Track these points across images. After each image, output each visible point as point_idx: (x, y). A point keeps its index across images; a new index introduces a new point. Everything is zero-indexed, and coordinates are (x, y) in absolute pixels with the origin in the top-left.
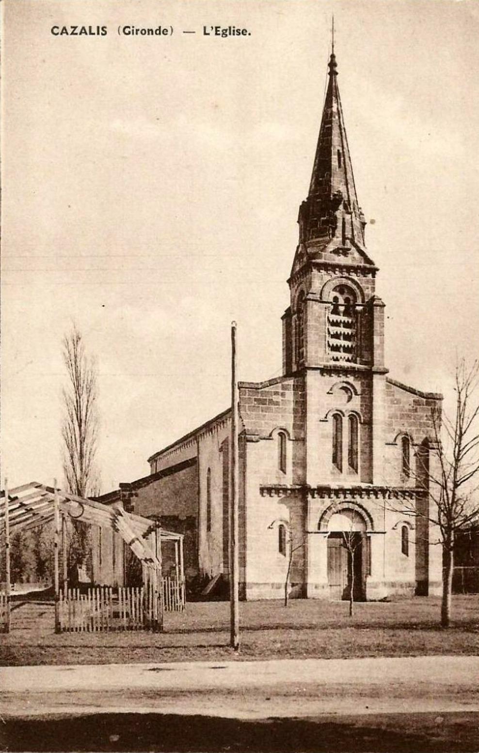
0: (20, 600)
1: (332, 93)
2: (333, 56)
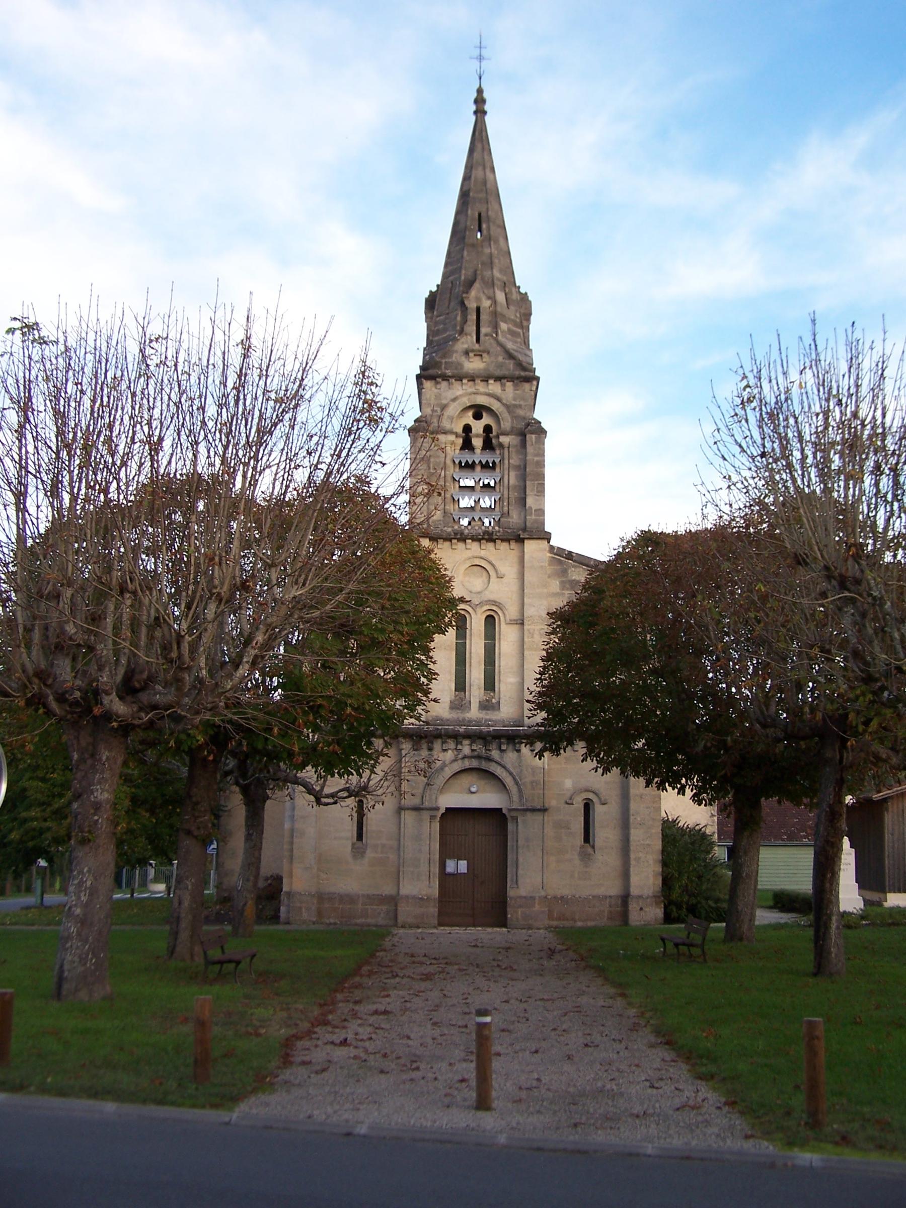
0: (840, 849)
1: (479, 138)
2: (480, 91)
